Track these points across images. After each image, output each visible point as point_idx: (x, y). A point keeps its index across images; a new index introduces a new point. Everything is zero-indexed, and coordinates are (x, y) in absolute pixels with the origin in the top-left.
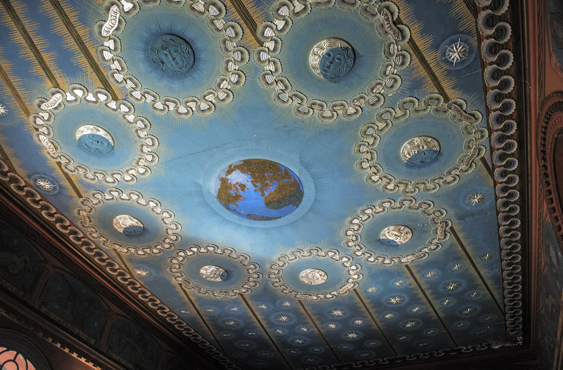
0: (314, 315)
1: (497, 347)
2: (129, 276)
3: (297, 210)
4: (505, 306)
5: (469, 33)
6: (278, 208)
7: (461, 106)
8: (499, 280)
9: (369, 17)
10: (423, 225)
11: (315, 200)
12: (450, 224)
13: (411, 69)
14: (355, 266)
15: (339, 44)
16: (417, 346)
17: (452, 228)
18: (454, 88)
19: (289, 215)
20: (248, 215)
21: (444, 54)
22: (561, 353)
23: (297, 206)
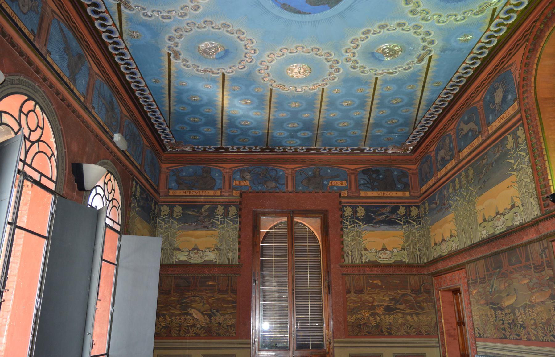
0: (275, 103)
1: (391, 152)
2: (117, 35)
3: (331, 10)
4: (420, 123)
6: (314, 6)
8: (431, 103)
10: (414, 49)
11: (350, 6)
16: (342, 105)
17: (430, 58)
19: (319, 14)
20: (284, 4)
22: (524, 355)
23: (331, 7)
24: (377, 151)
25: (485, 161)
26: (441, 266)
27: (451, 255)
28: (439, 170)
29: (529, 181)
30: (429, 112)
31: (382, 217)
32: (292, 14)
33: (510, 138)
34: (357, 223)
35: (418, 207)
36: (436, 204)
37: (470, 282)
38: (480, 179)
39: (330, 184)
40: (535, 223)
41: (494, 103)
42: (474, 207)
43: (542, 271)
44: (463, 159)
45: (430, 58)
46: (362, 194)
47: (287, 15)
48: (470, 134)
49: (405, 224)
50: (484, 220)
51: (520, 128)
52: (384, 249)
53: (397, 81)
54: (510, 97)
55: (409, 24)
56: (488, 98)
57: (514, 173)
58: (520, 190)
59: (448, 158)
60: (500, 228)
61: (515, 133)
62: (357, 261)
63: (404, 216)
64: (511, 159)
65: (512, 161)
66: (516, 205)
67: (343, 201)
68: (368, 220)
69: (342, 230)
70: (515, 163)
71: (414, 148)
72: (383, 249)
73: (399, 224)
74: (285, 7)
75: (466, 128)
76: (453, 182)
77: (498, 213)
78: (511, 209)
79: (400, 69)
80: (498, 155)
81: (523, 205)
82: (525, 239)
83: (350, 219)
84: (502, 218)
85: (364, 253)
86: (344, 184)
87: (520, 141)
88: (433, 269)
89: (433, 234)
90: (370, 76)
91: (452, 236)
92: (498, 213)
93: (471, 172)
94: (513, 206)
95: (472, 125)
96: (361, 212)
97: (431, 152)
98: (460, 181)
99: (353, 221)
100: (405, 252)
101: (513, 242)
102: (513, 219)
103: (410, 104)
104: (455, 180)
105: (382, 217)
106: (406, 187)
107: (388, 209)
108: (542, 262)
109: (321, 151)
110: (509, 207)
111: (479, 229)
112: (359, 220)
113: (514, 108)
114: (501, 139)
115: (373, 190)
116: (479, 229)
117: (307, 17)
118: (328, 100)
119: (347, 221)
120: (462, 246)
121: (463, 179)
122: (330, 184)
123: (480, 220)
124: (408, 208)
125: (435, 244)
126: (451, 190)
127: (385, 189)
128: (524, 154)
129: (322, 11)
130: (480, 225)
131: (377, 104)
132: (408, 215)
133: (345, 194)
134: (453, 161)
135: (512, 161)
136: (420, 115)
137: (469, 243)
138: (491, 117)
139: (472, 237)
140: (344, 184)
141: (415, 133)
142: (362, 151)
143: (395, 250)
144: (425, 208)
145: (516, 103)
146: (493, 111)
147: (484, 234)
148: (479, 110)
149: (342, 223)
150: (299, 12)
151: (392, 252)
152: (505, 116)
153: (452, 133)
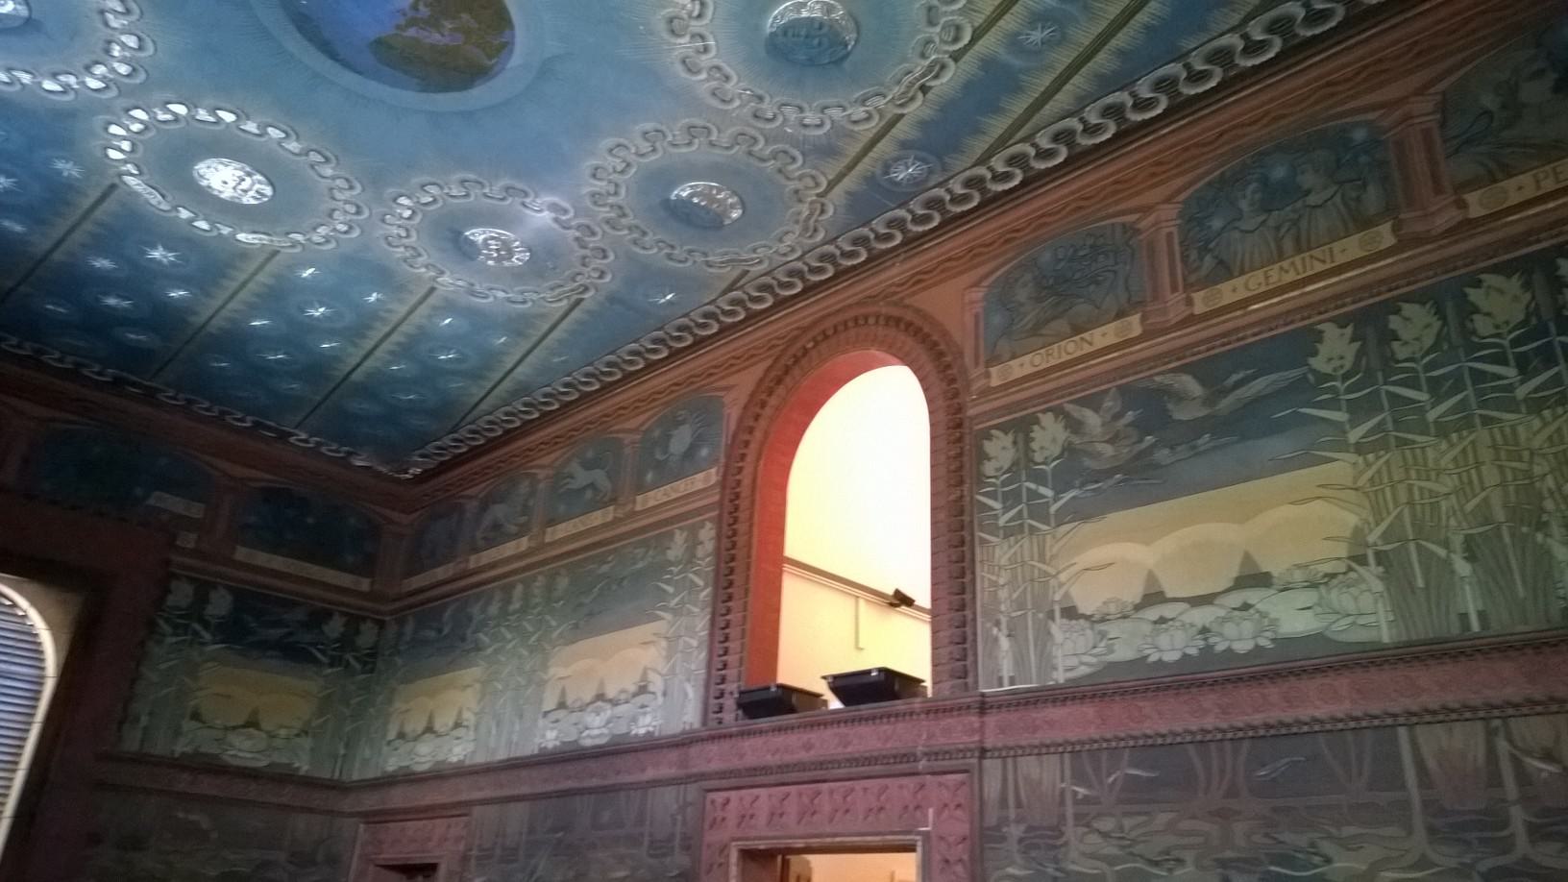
5: (944, 170)
7: (823, 212)
8: (523, 389)
9: (919, 49)
12: (586, 296)
13: (851, 135)
14: (140, 39)
15: (850, 37)
18: (848, 193)
21: (896, 160)
24: (323, 449)
25: (605, 568)
26: (397, 798)
27: (439, 775)
28: (475, 550)
29: (695, 643)
30: (508, 408)
31: (275, 633)
32: (312, 50)
33: (680, 538)
34: (196, 633)
35: (381, 625)
36: (440, 631)
37: (474, 853)
38: (581, 605)
39: (151, 502)
40: (683, 742)
41: (665, 450)
42: (545, 667)
43: (664, 855)
44: (552, 544)
45: (578, 302)
46: (241, 554)
47: (295, 44)
48: (589, 494)
49: (331, 665)
50: (562, 705)
51: (709, 525)
52: (252, 723)
53: (480, 320)
54: (704, 452)
55: (576, 216)
56: (657, 433)
57: (668, 616)
58: (668, 658)
59: (513, 529)
60: (596, 732)
61: (693, 531)
62: (159, 747)
63: (337, 641)
64: (668, 582)
65: (670, 589)
66: (651, 688)
67: (176, 558)
68: (234, 633)
69: (142, 643)
70: (674, 595)
71: (425, 471)
72: (248, 725)
73: (315, 661)
74: (304, 24)
75: (582, 477)
76: (508, 590)
77: (600, 697)
78: (635, 695)
79: (501, 294)
80: (640, 565)
81: (665, 694)
82: (650, 774)
83: (180, 617)
84: (608, 712)
85: (188, 725)
86: (196, 511)
87: (700, 552)
88: (370, 801)
89: (404, 707)
90: (419, 277)
91: (457, 725)
92: (600, 697)
93: (563, 583)
94: (643, 690)
95: (599, 476)
96: (220, 604)
97: (470, 497)
98: (527, 597)
99: (186, 627)
100: (307, 742)
101: (618, 773)
102: (634, 720)
103: (475, 375)
104: (512, 586)
105: (275, 633)
106: (367, 566)
107: (299, 614)
108: (673, 835)
109: (161, 397)
110: (633, 689)
111: (541, 722)
112: (206, 625)
113: (707, 479)
114: (658, 532)
115: (275, 548)
116: (541, 722)
117: (349, 78)
118: (271, 281)
119: (167, 620)
120: (480, 759)
121: (536, 591)
122: (151, 502)
123: (550, 703)
124: (354, 621)
125: (401, 735)
126: (493, 609)
127: (311, 558)
128: (701, 583)
129: (393, 85)
130: (546, 714)
131: (399, 344)
132: (346, 642)
133: (188, 540)
134: (525, 540)
135: (670, 589)
136: (483, 406)
137: (502, 755)
138: (649, 477)
139: (515, 738)
140: (196, 511)
141: (447, 441)
142: (283, 436)
143: (283, 732)
144: (400, 635)
145: (713, 471)
146: (659, 466)
147: (550, 738)
148: (628, 451)
149: (152, 626)
150: (333, 56)
151: (272, 736)
152: (682, 487)
153: (541, 474)
